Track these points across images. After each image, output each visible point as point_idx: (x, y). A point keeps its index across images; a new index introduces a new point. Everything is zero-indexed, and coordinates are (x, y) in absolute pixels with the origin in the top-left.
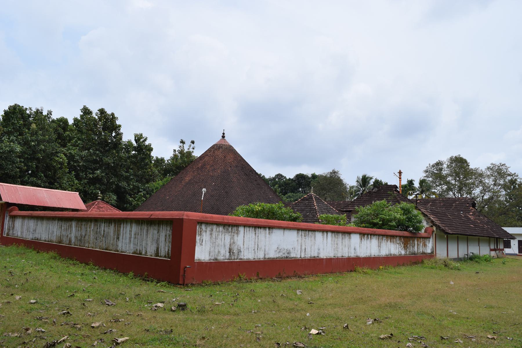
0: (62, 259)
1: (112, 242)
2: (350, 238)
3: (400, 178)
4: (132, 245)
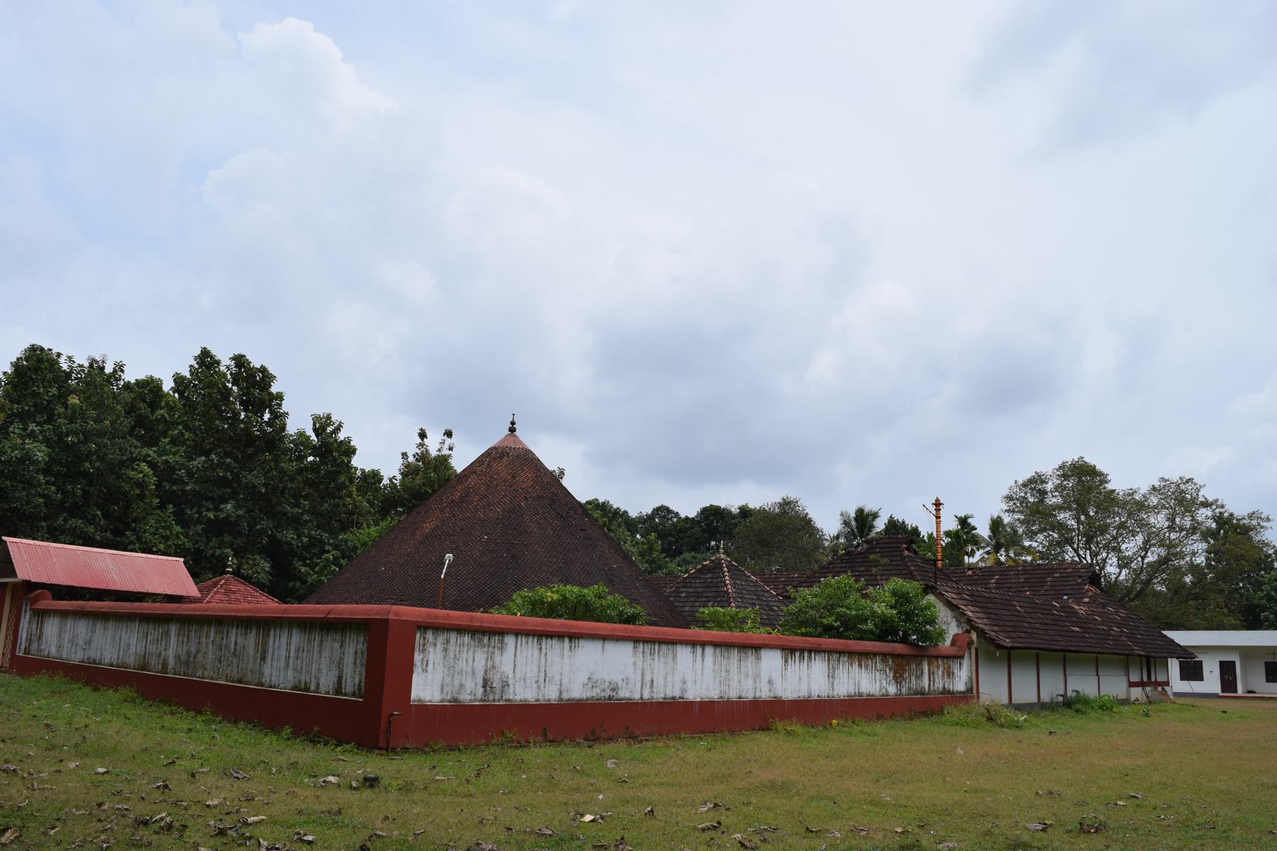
0: (146, 703)
1: (250, 666)
2: (758, 658)
3: (938, 517)
4: (290, 672)
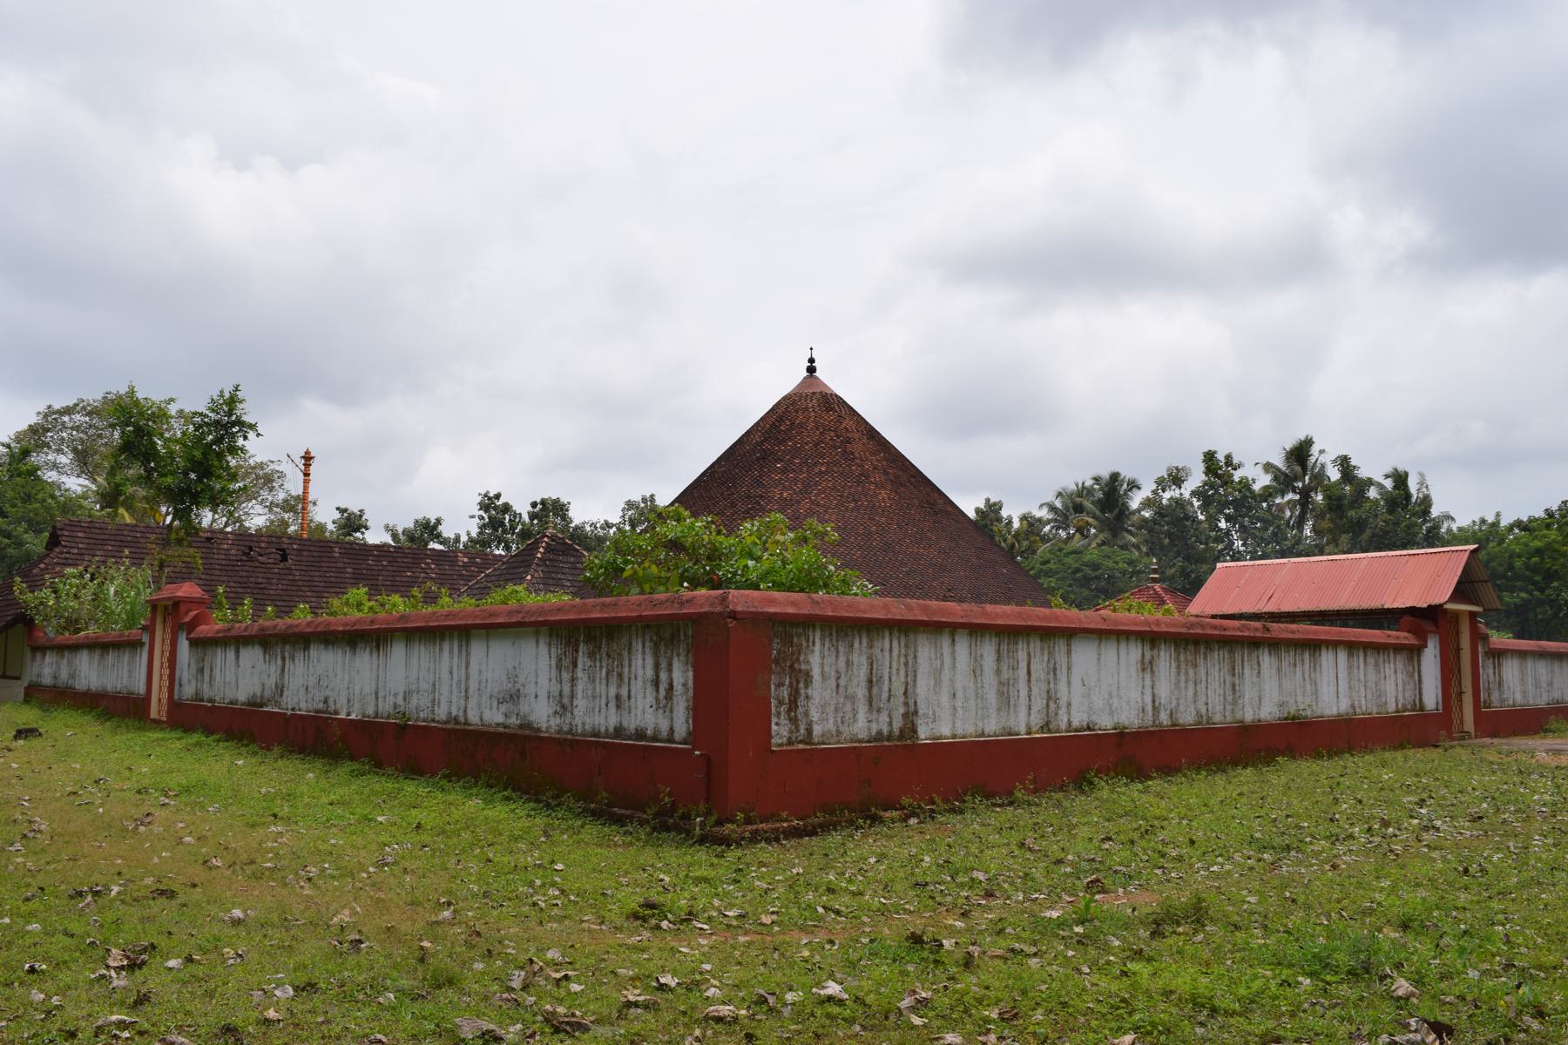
2: (1315, 666)
3: (307, 475)
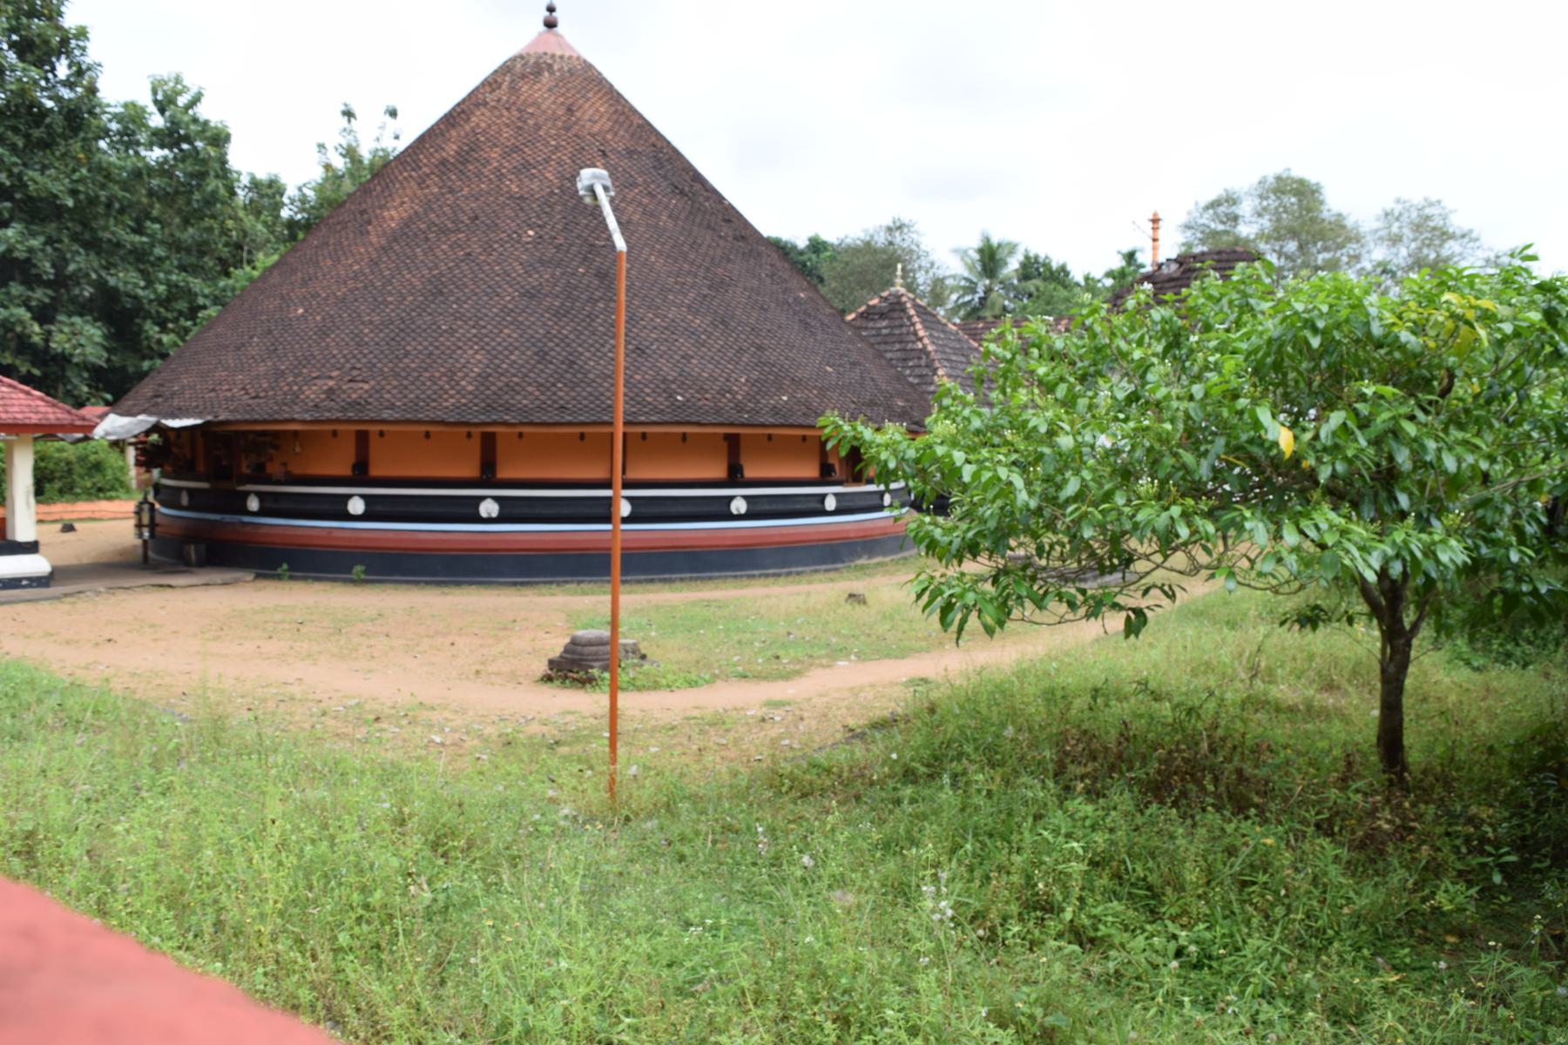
3: (1155, 240)
